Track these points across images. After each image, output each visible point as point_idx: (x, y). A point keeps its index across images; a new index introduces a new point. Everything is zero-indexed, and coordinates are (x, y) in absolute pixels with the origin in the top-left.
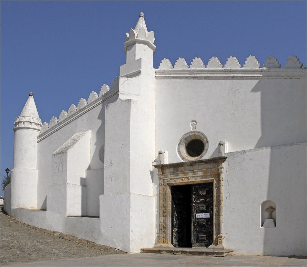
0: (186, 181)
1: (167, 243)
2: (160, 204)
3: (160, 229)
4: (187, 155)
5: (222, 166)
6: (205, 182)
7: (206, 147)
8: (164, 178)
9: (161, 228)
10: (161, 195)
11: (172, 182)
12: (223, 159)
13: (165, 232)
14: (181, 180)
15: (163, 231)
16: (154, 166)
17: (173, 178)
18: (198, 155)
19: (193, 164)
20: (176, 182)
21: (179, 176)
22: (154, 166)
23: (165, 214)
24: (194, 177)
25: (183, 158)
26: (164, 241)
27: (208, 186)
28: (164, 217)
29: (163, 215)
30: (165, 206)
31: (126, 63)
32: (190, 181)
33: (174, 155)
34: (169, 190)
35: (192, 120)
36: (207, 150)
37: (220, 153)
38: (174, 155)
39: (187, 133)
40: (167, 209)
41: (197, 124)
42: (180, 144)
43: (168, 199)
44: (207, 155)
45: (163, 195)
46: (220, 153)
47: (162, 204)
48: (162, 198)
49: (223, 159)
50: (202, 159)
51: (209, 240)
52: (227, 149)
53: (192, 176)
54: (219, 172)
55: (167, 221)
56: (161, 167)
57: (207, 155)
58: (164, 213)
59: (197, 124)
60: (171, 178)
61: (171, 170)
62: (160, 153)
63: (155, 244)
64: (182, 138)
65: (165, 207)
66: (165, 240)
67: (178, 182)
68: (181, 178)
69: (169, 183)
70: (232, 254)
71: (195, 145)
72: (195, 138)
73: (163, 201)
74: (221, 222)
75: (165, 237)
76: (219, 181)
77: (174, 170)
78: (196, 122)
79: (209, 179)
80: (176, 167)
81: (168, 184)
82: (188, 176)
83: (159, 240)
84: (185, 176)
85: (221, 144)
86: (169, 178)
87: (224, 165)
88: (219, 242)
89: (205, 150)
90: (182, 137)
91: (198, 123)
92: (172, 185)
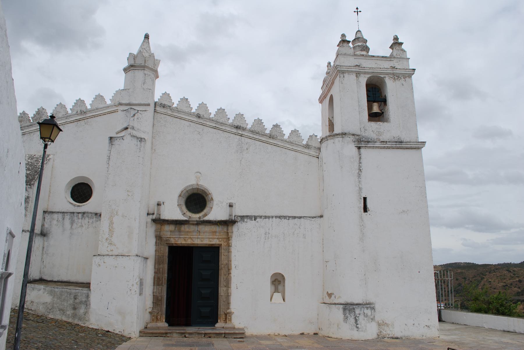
0: (189, 242)
7: (209, 205)
11: (173, 241)
14: (183, 239)
20: (177, 242)
24: (202, 238)
27: (213, 252)
33: (174, 211)
38: (174, 211)
44: (216, 212)
50: (206, 218)
56: (159, 222)
57: (216, 212)
61: (172, 227)
71: (196, 200)
79: (215, 242)
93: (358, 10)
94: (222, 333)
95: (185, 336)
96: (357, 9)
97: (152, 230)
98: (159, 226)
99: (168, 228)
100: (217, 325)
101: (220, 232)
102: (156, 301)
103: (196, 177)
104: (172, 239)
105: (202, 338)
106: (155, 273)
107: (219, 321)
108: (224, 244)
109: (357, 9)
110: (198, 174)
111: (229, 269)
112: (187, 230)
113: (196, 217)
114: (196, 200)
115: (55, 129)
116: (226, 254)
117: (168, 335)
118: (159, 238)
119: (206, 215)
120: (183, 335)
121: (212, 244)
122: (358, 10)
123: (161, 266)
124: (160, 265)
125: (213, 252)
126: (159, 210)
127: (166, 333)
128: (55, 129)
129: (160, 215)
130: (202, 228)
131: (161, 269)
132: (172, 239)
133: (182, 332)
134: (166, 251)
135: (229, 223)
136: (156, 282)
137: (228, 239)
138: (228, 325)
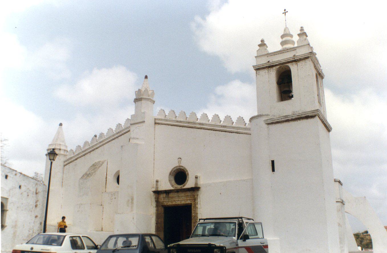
0: (174, 203)
11: (165, 204)
19: (177, 191)
21: (169, 199)
24: (180, 200)
25: (172, 186)
31: (131, 116)
33: (166, 185)
35: (178, 158)
36: (188, 180)
39: (175, 168)
44: (190, 184)
50: (185, 187)
53: (178, 200)
56: (157, 193)
57: (190, 184)
60: (164, 201)
61: (164, 195)
62: (64, 218)
68: (171, 201)
70: (235, 236)
71: (180, 176)
77: (166, 195)
78: (180, 158)
79: (189, 202)
80: (167, 192)
82: (175, 200)
86: (163, 201)
89: (187, 181)
93: (286, 11)
96: (285, 10)
97: (153, 196)
101: (190, 196)
104: (165, 202)
108: (193, 203)
109: (285, 10)
111: (157, 210)
112: (172, 196)
113: (179, 187)
114: (180, 176)
115: (55, 155)
116: (194, 209)
118: (157, 201)
119: (184, 186)
121: (187, 204)
122: (286, 11)
124: (159, 219)
128: (55, 155)
132: (165, 202)
134: (162, 210)
135: (196, 189)
137: (195, 200)
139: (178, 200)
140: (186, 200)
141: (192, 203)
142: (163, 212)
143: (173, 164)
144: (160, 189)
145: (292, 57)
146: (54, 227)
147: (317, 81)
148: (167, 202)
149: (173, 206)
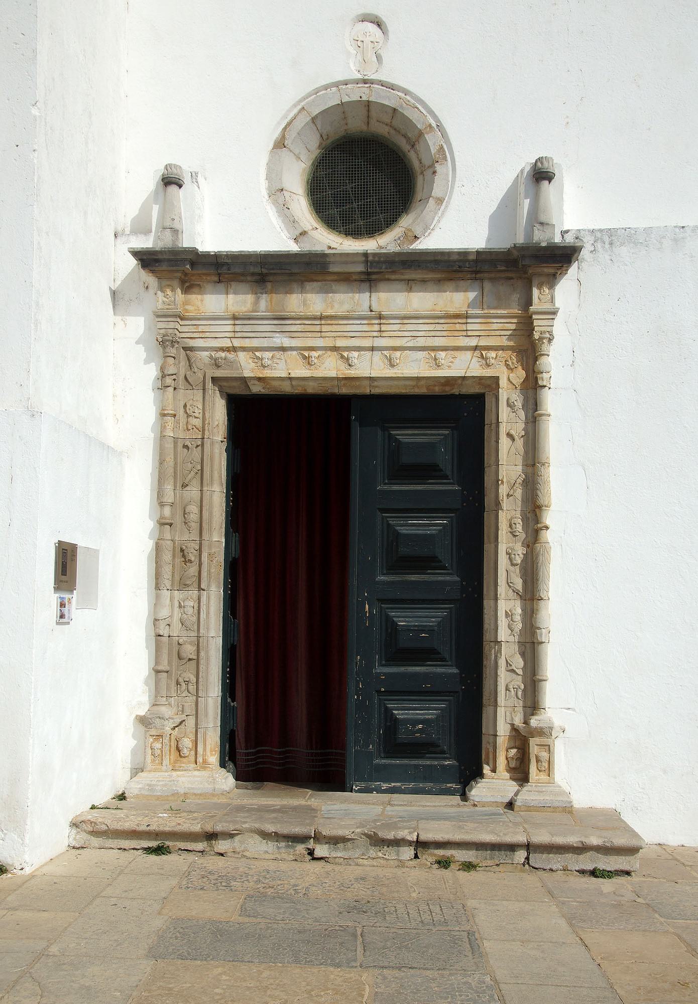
0: (329, 368)
1: (200, 760)
2: (162, 505)
3: (158, 672)
4: (315, 225)
5: (552, 300)
6: (437, 390)
8: (192, 343)
9: (164, 666)
10: (169, 445)
11: (247, 367)
12: (559, 258)
13: (192, 688)
15: (178, 683)
16: (136, 254)
17: (247, 343)
18: (373, 229)
20: (267, 373)
22: (136, 254)
23: (193, 570)
24: (388, 343)
26: (185, 752)
27: (457, 418)
28: (183, 585)
29: (177, 578)
30: (194, 516)
32: (352, 373)
34: (219, 413)
37: (542, 224)
38: (250, 206)
40: (205, 536)
41: (385, 32)
42: (280, 144)
43: (212, 477)
44: (459, 218)
45: (180, 445)
46: (536, 219)
47: (172, 505)
48: (174, 467)
49: (559, 258)
51: (456, 751)
52: (571, 213)
53: (367, 343)
54: (536, 336)
55: (203, 616)
56: (173, 266)
57: (459, 218)
58: (187, 561)
59: (385, 32)
60: (237, 343)
63: (137, 771)
64: (295, 111)
65: (195, 526)
66: (187, 743)
67: (279, 371)
69: (219, 373)
71: (366, 165)
72: (365, 128)
73: (184, 486)
74: (543, 636)
75: (191, 722)
76: (532, 387)
79: (461, 366)
81: (214, 380)
82: (340, 343)
83: (158, 745)
84: (329, 343)
85: (541, 175)
86: (227, 343)
87: (566, 293)
88: (538, 760)
90: (295, 106)
91: (391, 35)
92: (239, 390)
94: (512, 848)
95: (311, 853)
98: (541, 237)
99: (214, 302)
100: (479, 791)
102: (171, 662)
103: (359, 44)
105: (401, 864)
106: (162, 523)
107: (486, 770)
110: (372, 28)
114: (366, 165)
117: (222, 845)
118: (170, 345)
120: (301, 848)
121: (449, 381)
123: (193, 492)
125: (457, 418)
126: (167, 208)
127: (211, 836)
129: (175, 232)
130: (392, 300)
131: (194, 509)
132: (243, 358)
133: (297, 830)
135: (524, 267)
136: (167, 571)
137: (528, 349)
138: (528, 795)
139: (373, 349)
140: (445, 349)
141: (503, 382)
142: (616, 844)
143: (325, 65)
144: (209, 236)
145: (540, 275)
146: (166, 594)
147: (134, 834)
148: (268, 355)
149: (312, 389)
